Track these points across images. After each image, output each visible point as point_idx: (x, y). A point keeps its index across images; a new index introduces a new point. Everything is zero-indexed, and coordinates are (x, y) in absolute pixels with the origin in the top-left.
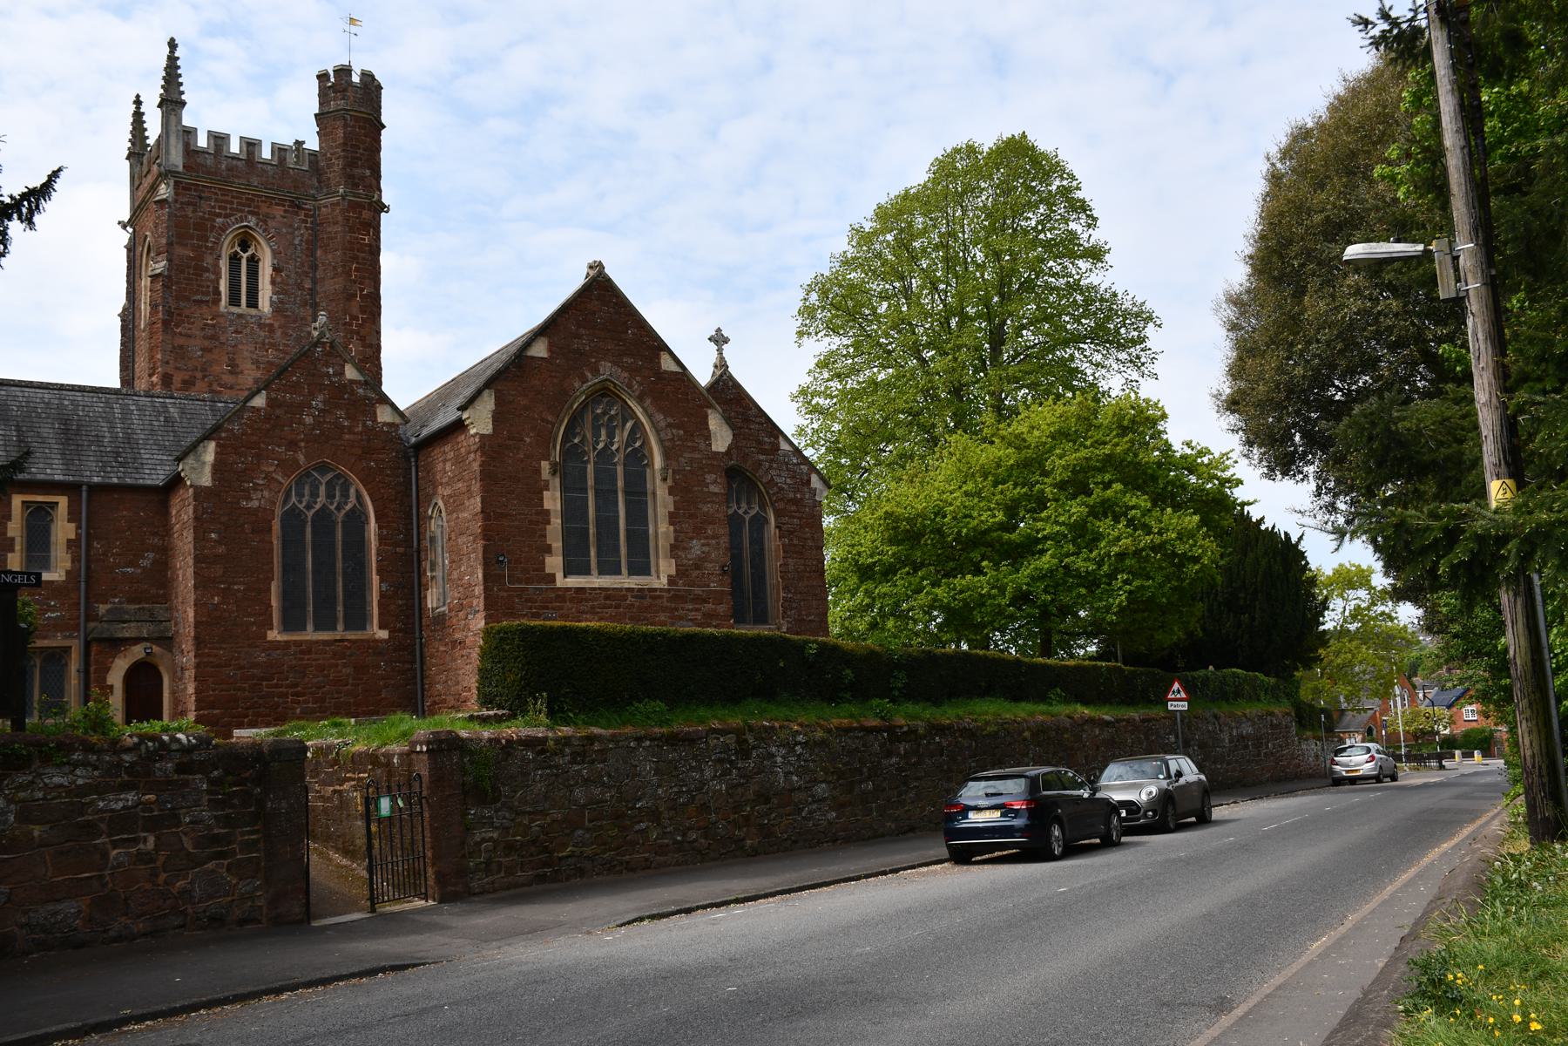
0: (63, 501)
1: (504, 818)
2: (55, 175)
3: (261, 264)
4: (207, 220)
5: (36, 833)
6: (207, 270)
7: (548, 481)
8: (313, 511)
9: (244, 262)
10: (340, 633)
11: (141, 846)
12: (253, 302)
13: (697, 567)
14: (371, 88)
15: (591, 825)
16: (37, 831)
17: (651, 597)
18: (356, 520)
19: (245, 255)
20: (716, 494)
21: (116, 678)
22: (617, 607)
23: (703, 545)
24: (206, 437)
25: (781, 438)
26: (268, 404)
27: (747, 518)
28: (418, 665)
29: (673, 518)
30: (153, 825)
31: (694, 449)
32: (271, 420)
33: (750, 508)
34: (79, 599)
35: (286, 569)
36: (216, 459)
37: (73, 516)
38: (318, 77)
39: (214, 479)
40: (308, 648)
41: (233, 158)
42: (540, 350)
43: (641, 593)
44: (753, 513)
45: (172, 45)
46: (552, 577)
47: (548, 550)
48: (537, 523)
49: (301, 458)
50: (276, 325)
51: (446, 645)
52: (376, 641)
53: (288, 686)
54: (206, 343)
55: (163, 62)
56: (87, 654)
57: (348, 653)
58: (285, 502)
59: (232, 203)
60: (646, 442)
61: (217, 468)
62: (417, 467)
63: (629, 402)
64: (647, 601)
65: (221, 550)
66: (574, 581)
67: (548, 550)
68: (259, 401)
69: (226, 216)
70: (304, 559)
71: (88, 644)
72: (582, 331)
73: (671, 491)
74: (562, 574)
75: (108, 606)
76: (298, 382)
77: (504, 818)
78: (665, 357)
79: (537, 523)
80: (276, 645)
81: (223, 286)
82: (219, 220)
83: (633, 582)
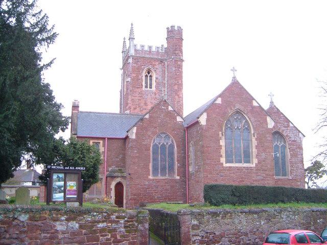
0: (101, 142)
2: (132, 25)
10: (167, 177)
13: (264, 161)
14: (180, 31)
16: (84, 231)
18: (172, 146)
21: (113, 186)
27: (280, 146)
30: (110, 231)
31: (263, 127)
35: (154, 160)
37: (104, 146)
40: (158, 181)
42: (219, 101)
43: (247, 168)
45: (132, 25)
46: (222, 164)
47: (221, 156)
54: (140, 98)
56: (106, 180)
58: (153, 143)
64: (249, 171)
65: (138, 155)
66: (228, 165)
67: (221, 156)
68: (147, 116)
71: (107, 177)
78: (254, 101)
80: (150, 180)
83: (246, 165)
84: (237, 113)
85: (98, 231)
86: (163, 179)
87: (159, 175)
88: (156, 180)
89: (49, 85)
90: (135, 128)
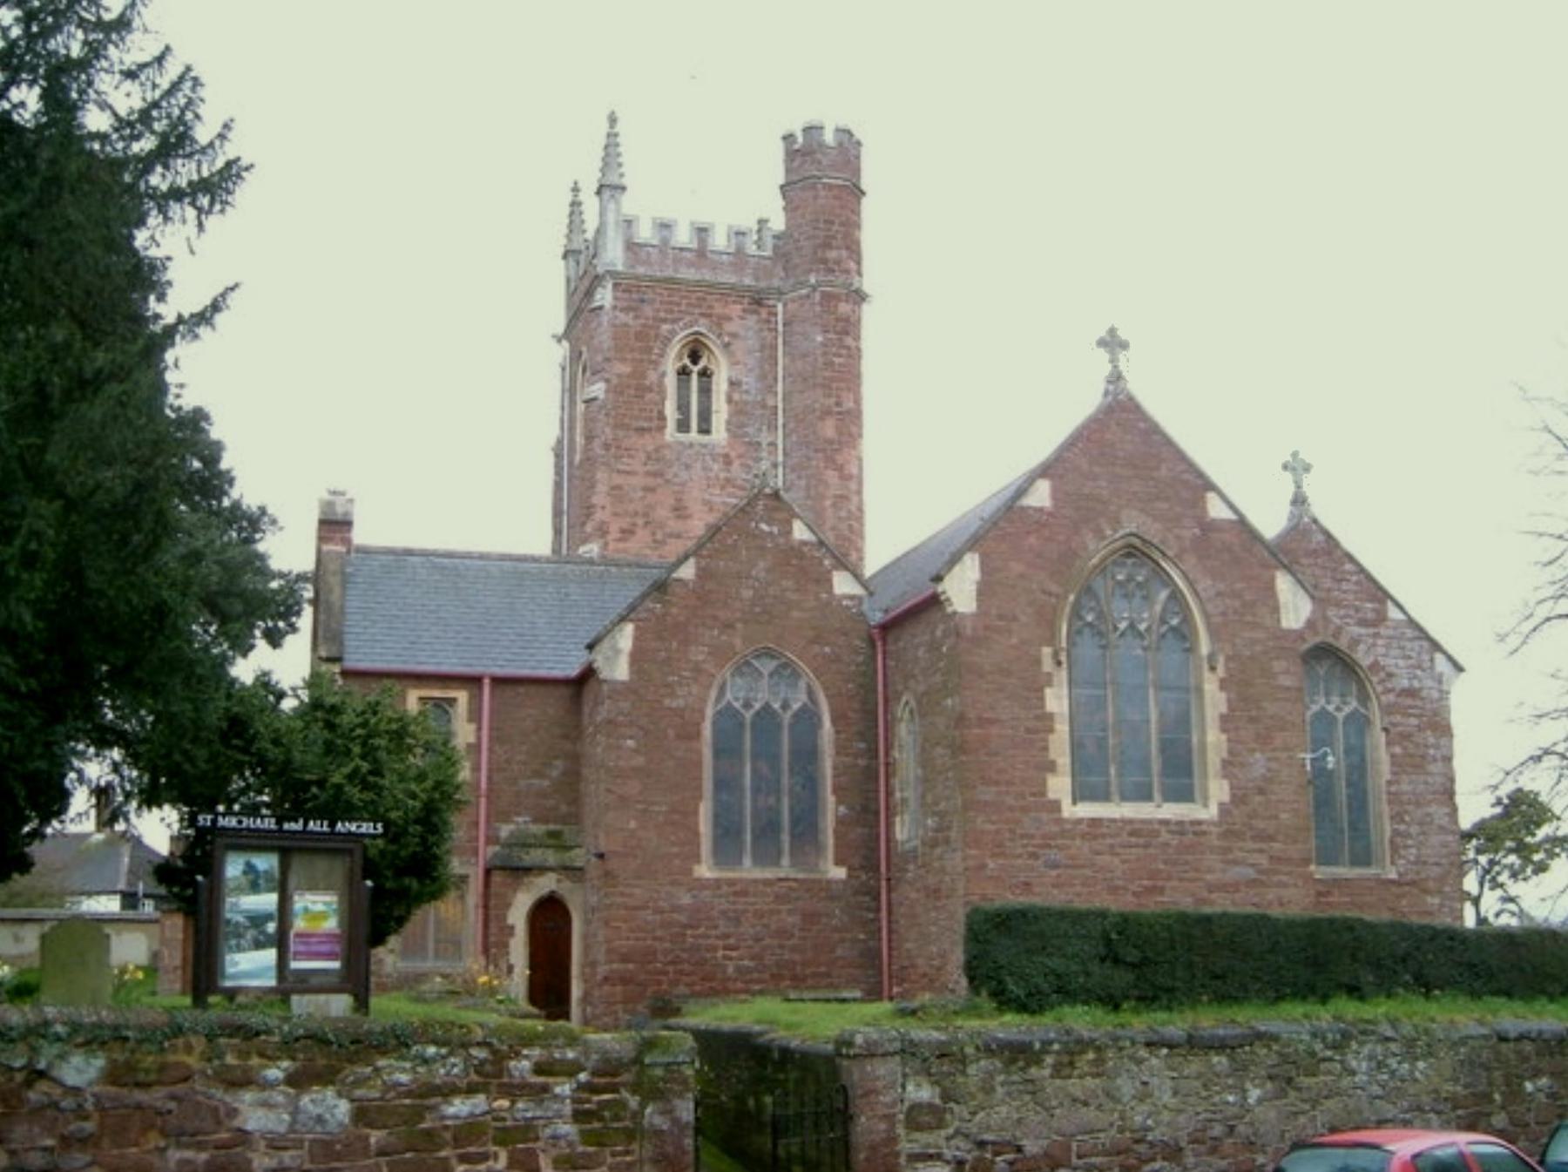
0: (462, 696)
1: (958, 1149)
3: (714, 378)
4: (651, 327)
5: (373, 1140)
6: (650, 389)
7: (1049, 674)
8: (752, 712)
9: (694, 377)
10: (785, 869)
11: (491, 1163)
12: (705, 429)
14: (848, 150)
15: (1081, 1162)
17: (1195, 833)
18: (808, 717)
19: (696, 369)
20: (1288, 689)
22: (1146, 846)
23: (1269, 760)
24: (623, 619)
25: (1390, 604)
26: (697, 575)
27: (1340, 716)
28: (884, 914)
29: (1226, 722)
31: (1255, 626)
32: (702, 592)
33: (1345, 703)
34: (478, 815)
35: (720, 785)
36: (634, 645)
37: (475, 715)
38: (785, 138)
39: (632, 672)
40: (741, 890)
41: (681, 249)
43: (1179, 828)
44: (1347, 710)
45: (613, 120)
47: (1051, 767)
48: (1036, 731)
49: (738, 642)
50: (733, 454)
51: (918, 891)
52: (829, 882)
53: (717, 937)
54: (650, 481)
55: (602, 141)
57: (794, 895)
59: (679, 304)
60: (1187, 618)
61: (637, 657)
62: (885, 653)
63: (1164, 564)
65: (640, 761)
66: (1086, 810)
67: (1051, 767)
68: (687, 571)
69: (674, 321)
70: (741, 775)
72: (1096, 469)
73: (1223, 685)
74: (1069, 800)
75: (512, 827)
76: (735, 546)
77: (958, 1149)
78: (1212, 498)
79: (1036, 731)
80: (703, 884)
81: (670, 410)
82: (665, 327)
83: (1171, 811)
86: (767, 882)
87: (747, 861)
90: (629, 628)
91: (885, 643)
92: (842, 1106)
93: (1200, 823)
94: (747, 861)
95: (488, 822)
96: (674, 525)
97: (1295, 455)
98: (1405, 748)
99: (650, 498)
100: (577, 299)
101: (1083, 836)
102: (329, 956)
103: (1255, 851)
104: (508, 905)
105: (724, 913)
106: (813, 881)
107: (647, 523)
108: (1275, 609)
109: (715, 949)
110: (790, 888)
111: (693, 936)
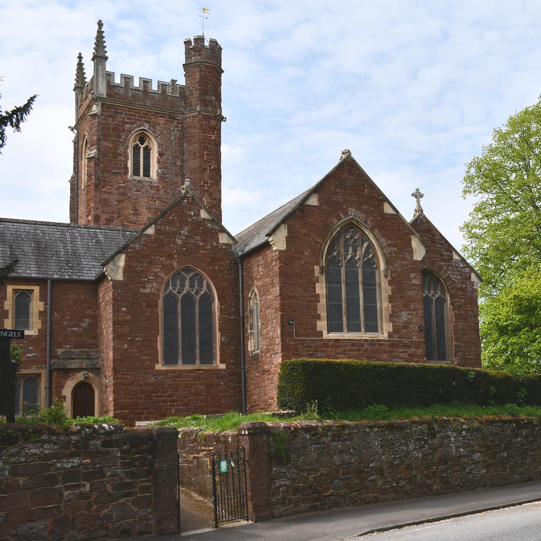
0: (36, 289)
1: (293, 473)
3: (151, 151)
6: (120, 155)
10: (197, 365)
12: (147, 173)
15: (343, 477)
18: (207, 300)
19: (142, 146)
20: (416, 285)
21: (67, 391)
23: (408, 314)
24: (120, 252)
25: (454, 253)
26: (156, 233)
27: (434, 298)
28: (243, 384)
29: (391, 299)
30: (89, 477)
31: (404, 259)
33: (436, 293)
34: (46, 345)
37: (43, 298)
39: (124, 276)
40: (179, 374)
41: (135, 90)
42: (314, 201)
43: (372, 342)
44: (437, 296)
45: (100, 24)
47: (319, 317)
48: (312, 302)
49: (175, 264)
50: (160, 186)
52: (218, 370)
54: (120, 197)
59: (135, 116)
61: (127, 270)
63: (365, 232)
64: (376, 347)
65: (129, 317)
66: (333, 336)
67: (319, 317)
68: (151, 231)
72: (338, 190)
75: (63, 350)
79: (312, 302)
80: (160, 372)
84: (350, 228)
85: (60, 478)
86: (189, 371)
87: (180, 362)
88: (173, 372)
89: (200, 40)
90: (123, 257)
91: (242, 263)
92: (243, 457)
93: (381, 340)
94: (180, 362)
95: (50, 348)
96: (133, 218)
97: (418, 190)
98: (459, 311)
99: (121, 205)
100: (82, 111)
101: (332, 347)
102: (17, 374)
103: (402, 352)
104: (63, 387)
105: (169, 386)
106: (211, 370)
107: (119, 217)
108: (411, 252)
109: (166, 402)
110: (201, 374)
111: (156, 397)
